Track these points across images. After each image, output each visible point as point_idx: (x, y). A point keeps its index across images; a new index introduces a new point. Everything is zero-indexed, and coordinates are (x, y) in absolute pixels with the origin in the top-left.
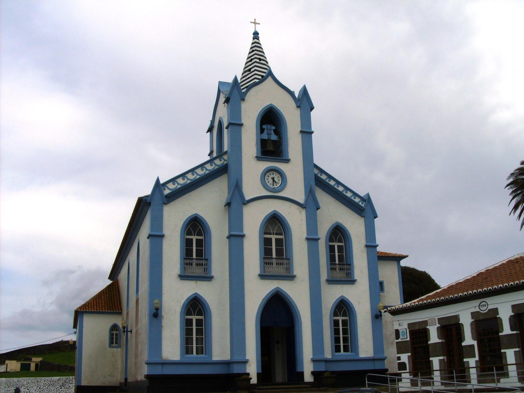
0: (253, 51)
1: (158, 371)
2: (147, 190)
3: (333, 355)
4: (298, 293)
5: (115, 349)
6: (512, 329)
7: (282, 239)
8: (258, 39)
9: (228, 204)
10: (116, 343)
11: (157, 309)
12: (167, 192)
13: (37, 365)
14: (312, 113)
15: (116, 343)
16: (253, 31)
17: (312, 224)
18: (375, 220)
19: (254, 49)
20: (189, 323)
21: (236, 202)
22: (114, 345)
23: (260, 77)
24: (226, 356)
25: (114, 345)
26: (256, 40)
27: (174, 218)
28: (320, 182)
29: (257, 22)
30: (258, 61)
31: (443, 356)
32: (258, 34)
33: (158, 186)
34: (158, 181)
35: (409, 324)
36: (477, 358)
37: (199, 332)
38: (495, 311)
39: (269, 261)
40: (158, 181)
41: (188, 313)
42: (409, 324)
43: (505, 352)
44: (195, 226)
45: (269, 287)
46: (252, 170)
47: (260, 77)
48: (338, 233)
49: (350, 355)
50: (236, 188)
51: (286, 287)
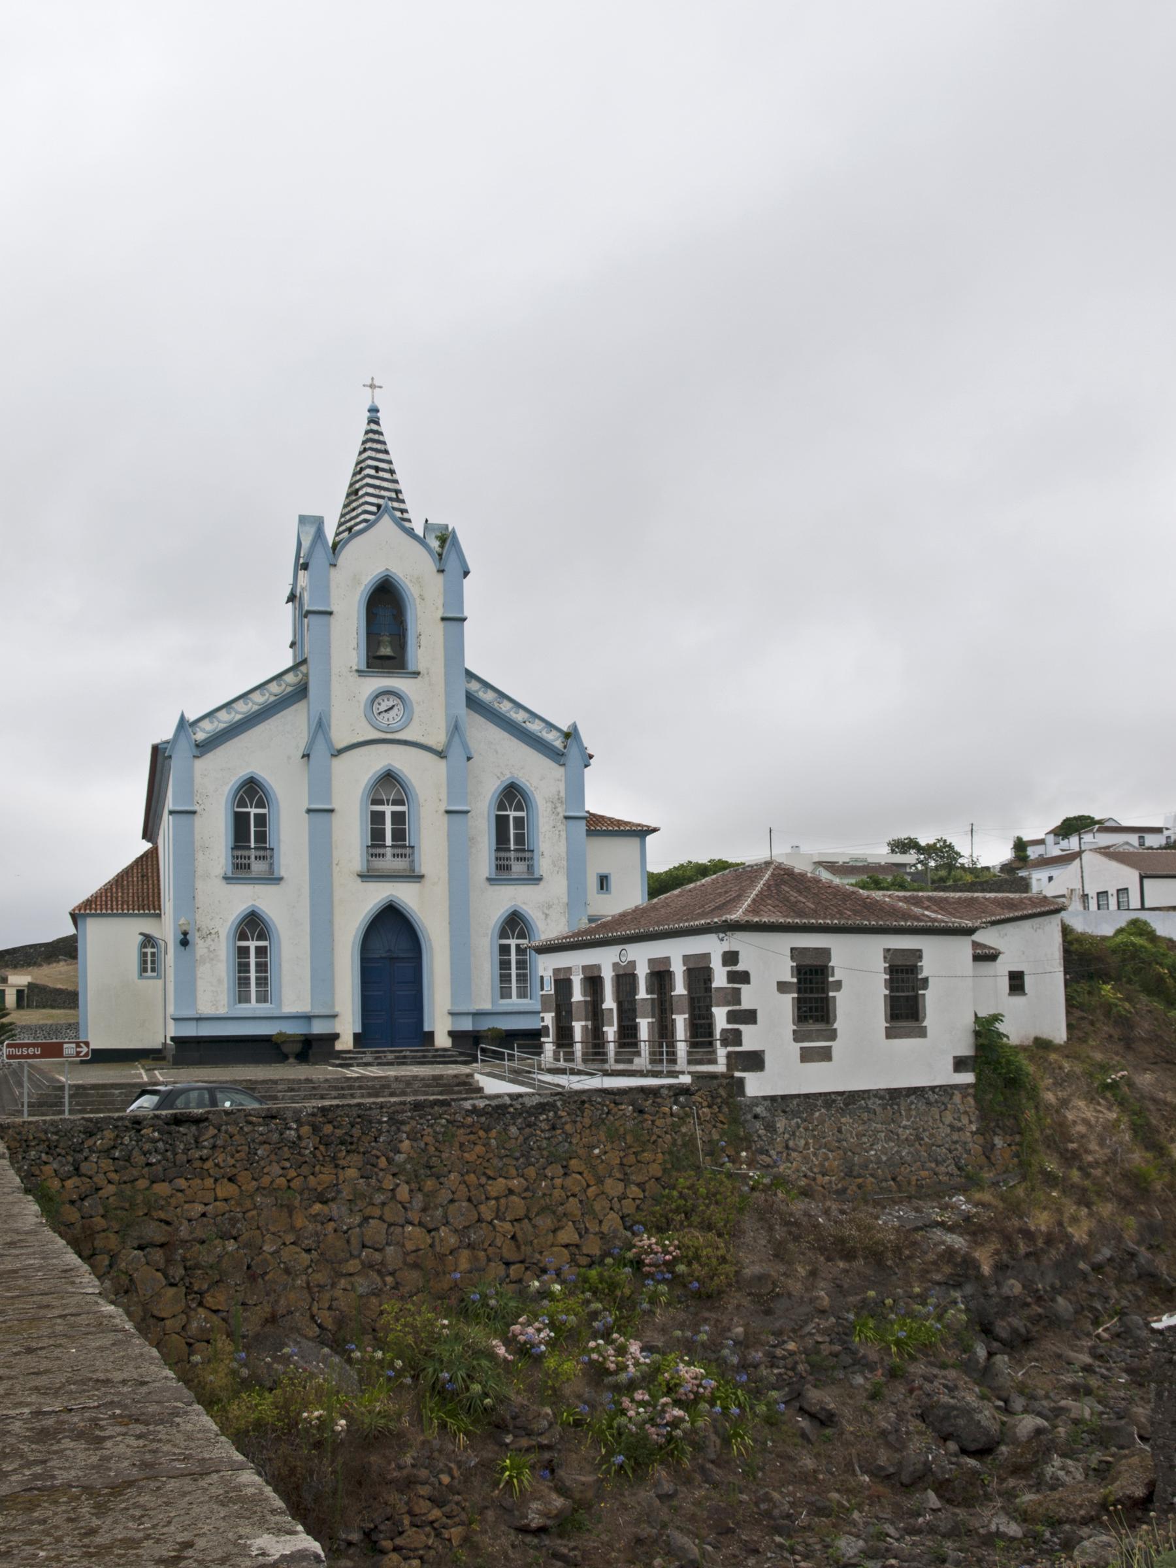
0: (365, 450)
1: (190, 1031)
2: (165, 732)
3: (493, 1003)
4: (427, 906)
5: (151, 982)
6: (648, 993)
7: (404, 813)
8: (377, 423)
9: (306, 756)
10: (153, 970)
11: (185, 934)
12: (200, 736)
13: (20, 993)
14: (467, 582)
15: (153, 970)
16: (368, 406)
17: (457, 785)
18: (586, 770)
19: (368, 445)
20: (243, 952)
21: (320, 749)
22: (149, 974)
23: (374, 509)
24: (303, 1006)
25: (149, 974)
26: (374, 427)
27: (212, 783)
28: (481, 703)
29: (377, 383)
30: (372, 472)
31: (586, 1020)
32: (377, 411)
33: (183, 725)
34: (182, 718)
35: (555, 970)
36: (615, 1028)
37: (262, 967)
38: (633, 964)
39: (381, 851)
40: (182, 718)
41: (243, 936)
42: (555, 970)
43: (834, 997)
44: (251, 790)
45: (377, 895)
46: (348, 691)
47: (374, 509)
48: (513, 795)
49: (528, 1004)
50: (321, 727)
51: (406, 895)
